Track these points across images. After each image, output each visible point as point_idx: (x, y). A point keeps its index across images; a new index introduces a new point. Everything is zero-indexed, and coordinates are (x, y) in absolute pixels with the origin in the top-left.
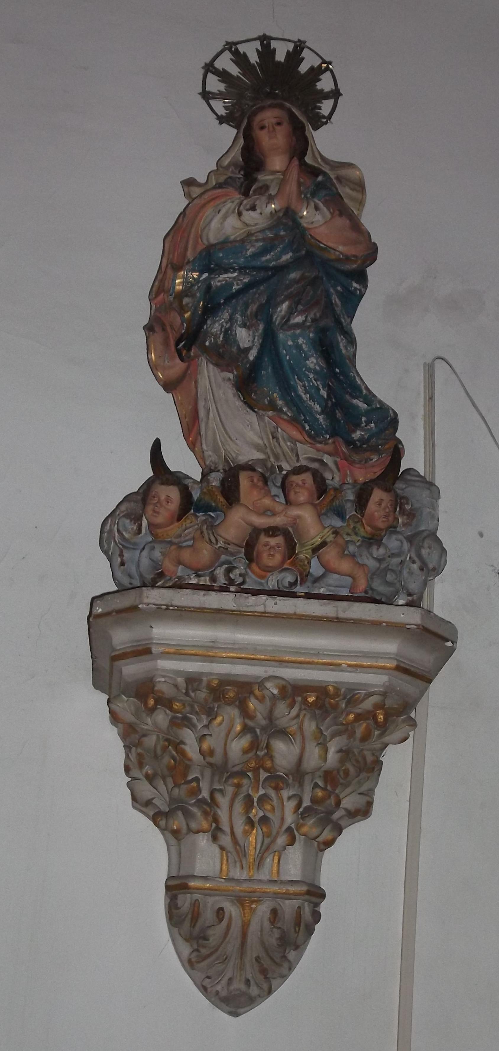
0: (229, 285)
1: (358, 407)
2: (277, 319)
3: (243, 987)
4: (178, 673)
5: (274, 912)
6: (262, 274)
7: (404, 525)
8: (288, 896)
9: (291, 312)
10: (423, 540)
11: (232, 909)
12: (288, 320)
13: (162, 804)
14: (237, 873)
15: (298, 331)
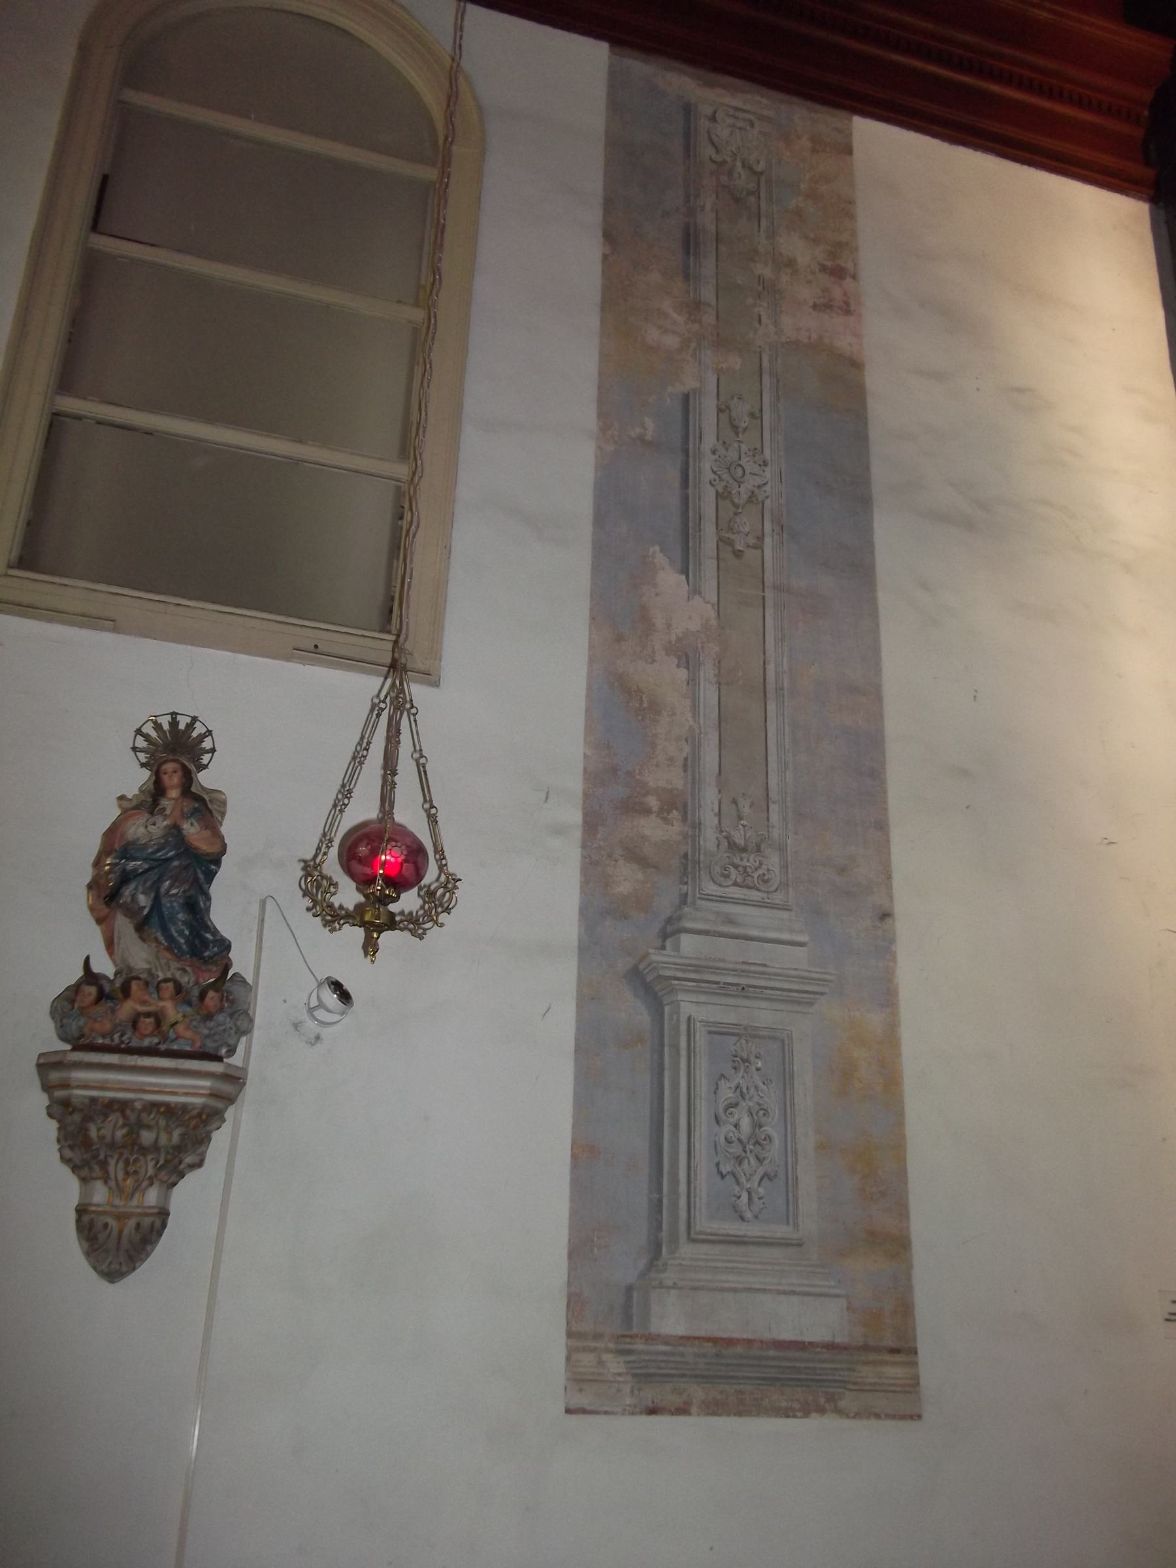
0: (136, 869)
1: (207, 938)
2: (163, 890)
3: (118, 1267)
4: (85, 1097)
5: (138, 1225)
6: (156, 863)
7: (228, 1007)
8: (146, 1215)
9: (171, 887)
10: (239, 1016)
11: (113, 1223)
12: (168, 892)
13: (77, 1161)
14: (117, 1202)
15: (173, 899)
